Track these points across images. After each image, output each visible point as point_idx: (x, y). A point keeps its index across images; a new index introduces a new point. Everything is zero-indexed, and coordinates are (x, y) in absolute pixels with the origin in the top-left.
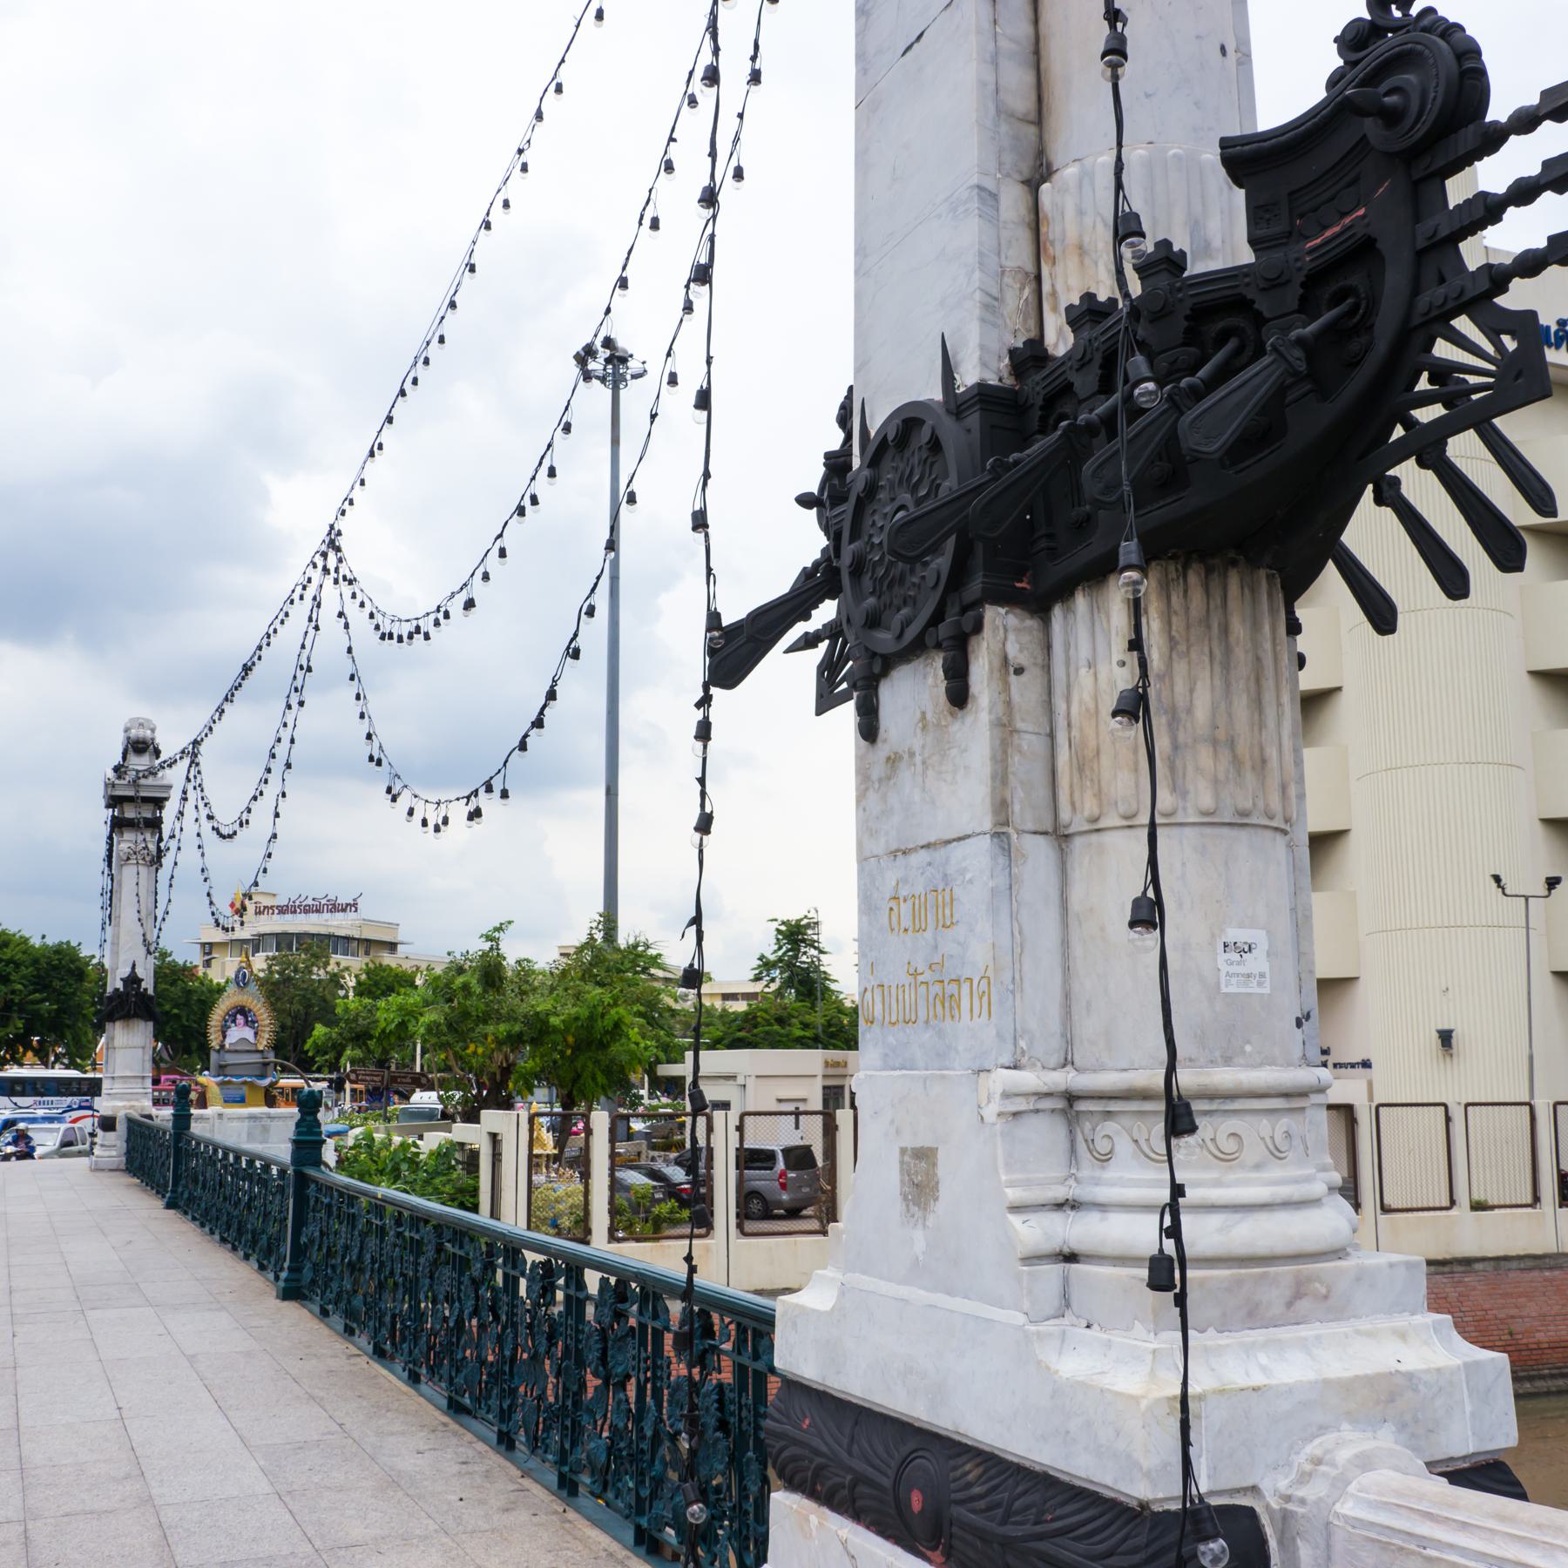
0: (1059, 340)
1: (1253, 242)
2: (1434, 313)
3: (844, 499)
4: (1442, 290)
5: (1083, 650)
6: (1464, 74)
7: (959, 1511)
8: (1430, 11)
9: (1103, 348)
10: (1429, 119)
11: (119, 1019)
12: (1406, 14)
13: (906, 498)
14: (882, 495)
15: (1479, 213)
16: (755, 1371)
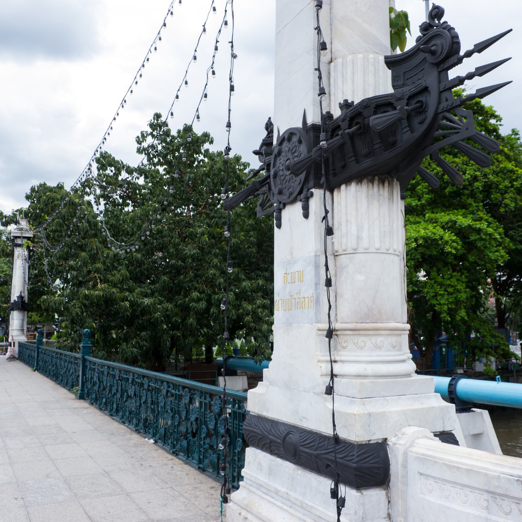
0: (337, 113)
1: (394, 87)
2: (445, 109)
3: (271, 154)
4: (447, 103)
5: (343, 203)
6: (453, 43)
7: (301, 448)
8: (445, 22)
9: (350, 115)
10: (445, 52)
11: (16, 310)
12: (439, 22)
13: (290, 156)
14: (283, 154)
15: (457, 82)
16: (205, 403)
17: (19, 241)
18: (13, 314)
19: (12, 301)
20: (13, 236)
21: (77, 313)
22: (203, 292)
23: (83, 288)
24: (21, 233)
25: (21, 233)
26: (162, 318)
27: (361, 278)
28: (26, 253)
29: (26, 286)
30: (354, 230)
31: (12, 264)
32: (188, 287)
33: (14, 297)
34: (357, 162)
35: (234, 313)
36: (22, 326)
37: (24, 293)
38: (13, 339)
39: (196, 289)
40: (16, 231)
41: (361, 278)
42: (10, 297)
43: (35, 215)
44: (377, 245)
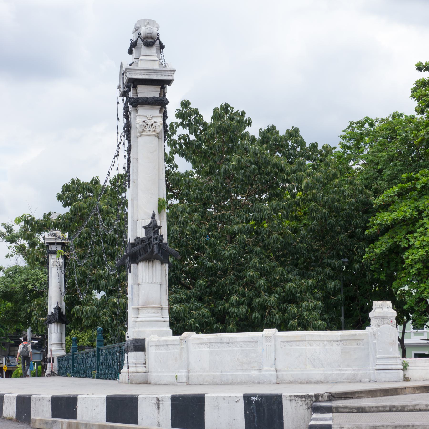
11: (53, 323)
17: (53, 248)
18: (51, 327)
19: (49, 313)
20: (47, 243)
21: (107, 321)
22: (244, 295)
23: (113, 297)
24: (55, 239)
25: (55, 239)
26: (197, 325)
27: (143, 292)
28: (61, 260)
29: (63, 297)
30: (141, 277)
31: (48, 274)
32: (229, 290)
33: (51, 309)
34: (141, 256)
35: (278, 318)
36: (61, 340)
37: (61, 304)
38: (51, 354)
39: (236, 292)
40: (50, 237)
41: (143, 292)
42: (47, 309)
43: (64, 226)
44: (155, 281)
